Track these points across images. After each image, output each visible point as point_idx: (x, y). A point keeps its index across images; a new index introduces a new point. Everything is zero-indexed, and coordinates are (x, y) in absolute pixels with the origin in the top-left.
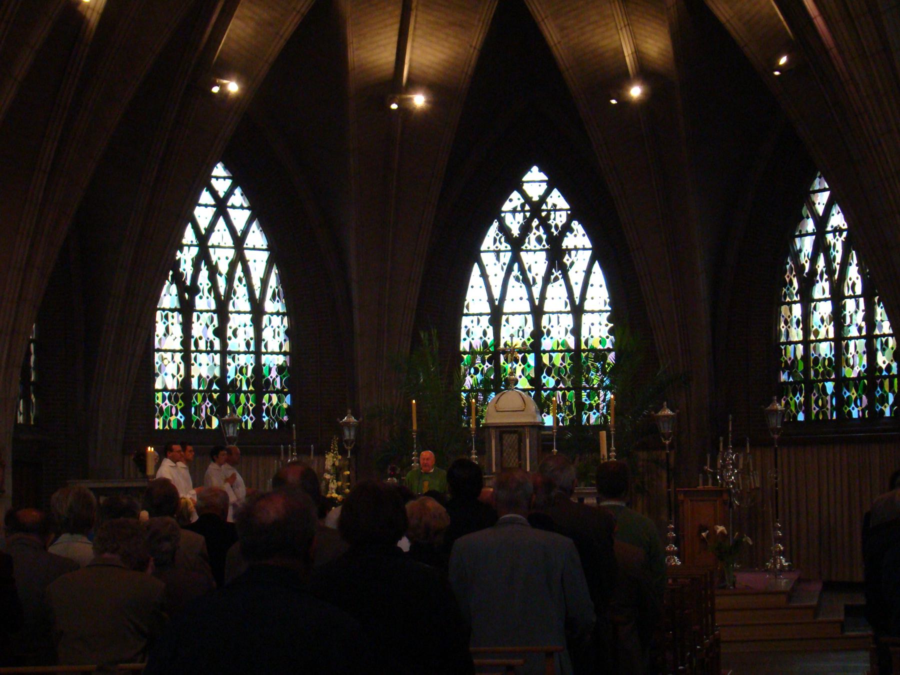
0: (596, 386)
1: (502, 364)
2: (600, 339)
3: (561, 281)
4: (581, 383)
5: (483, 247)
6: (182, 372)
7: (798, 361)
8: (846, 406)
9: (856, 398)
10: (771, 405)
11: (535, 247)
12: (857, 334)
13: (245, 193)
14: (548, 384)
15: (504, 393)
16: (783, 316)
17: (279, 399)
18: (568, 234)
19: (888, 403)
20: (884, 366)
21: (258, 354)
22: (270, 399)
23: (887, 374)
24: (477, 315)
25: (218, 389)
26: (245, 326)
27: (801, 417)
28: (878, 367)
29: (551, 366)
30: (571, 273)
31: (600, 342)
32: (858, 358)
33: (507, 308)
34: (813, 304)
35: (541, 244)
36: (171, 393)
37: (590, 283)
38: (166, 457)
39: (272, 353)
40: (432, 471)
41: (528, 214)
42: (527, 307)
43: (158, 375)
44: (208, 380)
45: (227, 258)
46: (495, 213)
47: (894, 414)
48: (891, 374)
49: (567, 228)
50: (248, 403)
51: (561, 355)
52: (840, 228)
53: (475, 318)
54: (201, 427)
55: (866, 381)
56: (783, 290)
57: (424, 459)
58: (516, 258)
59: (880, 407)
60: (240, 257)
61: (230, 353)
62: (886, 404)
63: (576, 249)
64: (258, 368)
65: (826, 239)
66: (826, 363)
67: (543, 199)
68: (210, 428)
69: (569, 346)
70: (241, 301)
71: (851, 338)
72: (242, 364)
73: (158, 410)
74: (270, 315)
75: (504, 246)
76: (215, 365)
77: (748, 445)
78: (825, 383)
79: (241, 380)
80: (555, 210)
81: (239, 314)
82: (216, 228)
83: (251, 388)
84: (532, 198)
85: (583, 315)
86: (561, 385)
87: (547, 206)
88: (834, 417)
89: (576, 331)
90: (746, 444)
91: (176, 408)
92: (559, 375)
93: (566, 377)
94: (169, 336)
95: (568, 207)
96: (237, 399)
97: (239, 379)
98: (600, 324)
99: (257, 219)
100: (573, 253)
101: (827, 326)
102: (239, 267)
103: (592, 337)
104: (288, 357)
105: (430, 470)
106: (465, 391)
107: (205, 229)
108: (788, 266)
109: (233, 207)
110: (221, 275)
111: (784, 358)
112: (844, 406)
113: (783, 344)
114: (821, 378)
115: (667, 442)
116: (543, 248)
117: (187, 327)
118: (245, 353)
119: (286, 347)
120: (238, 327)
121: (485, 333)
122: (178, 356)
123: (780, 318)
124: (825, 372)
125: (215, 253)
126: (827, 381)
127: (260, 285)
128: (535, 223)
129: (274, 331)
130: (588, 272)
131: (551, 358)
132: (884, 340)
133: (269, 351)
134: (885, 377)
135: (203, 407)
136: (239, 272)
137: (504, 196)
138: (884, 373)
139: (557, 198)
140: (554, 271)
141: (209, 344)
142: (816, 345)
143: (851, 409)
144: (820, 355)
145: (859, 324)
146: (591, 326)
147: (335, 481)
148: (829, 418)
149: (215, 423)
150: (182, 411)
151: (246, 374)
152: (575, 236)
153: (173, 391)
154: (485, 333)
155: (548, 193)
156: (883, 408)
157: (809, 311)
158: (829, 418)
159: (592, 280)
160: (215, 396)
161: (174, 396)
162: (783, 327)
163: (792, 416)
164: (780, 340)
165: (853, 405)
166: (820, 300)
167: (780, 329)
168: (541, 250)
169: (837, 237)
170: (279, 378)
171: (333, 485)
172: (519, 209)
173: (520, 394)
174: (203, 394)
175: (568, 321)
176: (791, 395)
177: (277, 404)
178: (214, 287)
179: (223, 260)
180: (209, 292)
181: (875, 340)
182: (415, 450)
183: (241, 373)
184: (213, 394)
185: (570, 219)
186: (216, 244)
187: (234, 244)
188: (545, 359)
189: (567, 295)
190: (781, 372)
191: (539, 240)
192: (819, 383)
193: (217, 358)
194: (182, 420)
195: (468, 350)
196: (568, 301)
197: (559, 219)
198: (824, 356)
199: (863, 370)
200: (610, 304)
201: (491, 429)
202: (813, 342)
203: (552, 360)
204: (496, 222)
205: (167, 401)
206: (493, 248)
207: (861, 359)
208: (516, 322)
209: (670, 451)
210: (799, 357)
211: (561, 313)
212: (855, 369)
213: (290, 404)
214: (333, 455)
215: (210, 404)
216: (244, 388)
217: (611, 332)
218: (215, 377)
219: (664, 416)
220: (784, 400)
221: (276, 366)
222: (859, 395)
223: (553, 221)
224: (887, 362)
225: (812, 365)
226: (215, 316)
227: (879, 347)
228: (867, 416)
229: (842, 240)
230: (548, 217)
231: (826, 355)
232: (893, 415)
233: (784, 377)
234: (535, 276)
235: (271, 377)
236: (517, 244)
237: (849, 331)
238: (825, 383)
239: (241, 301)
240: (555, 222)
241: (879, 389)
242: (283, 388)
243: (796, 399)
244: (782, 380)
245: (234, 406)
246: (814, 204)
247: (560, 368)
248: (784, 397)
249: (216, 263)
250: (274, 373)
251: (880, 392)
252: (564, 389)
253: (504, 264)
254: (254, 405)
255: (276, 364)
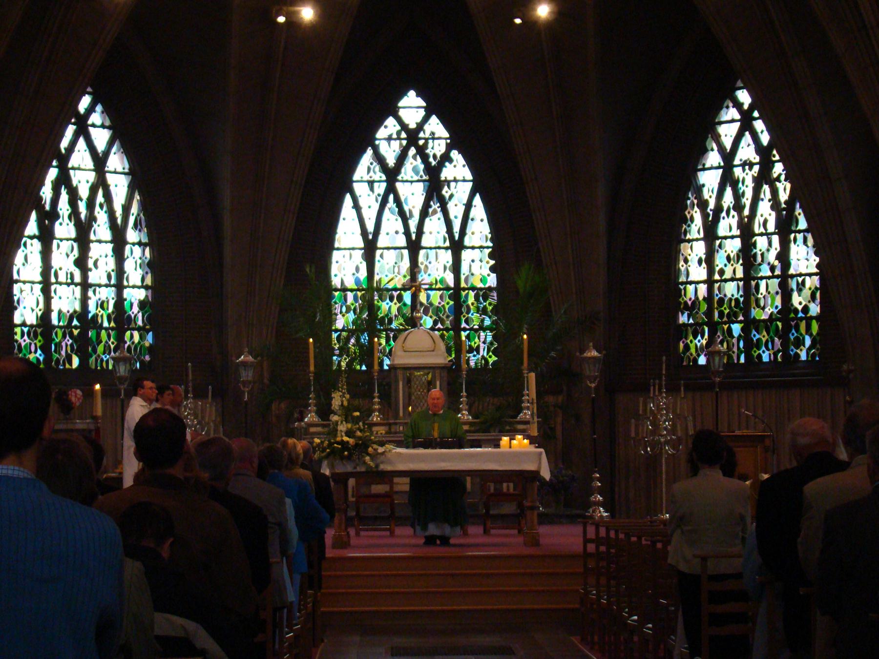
0: (476, 327)
1: (376, 302)
2: (481, 276)
3: (440, 215)
4: (460, 324)
5: (356, 177)
6: (41, 306)
7: (699, 302)
8: (755, 349)
9: (767, 341)
10: (712, 346)
11: (412, 177)
12: (769, 274)
13: (106, 111)
14: (426, 324)
15: (411, 332)
16: (683, 255)
17: (141, 337)
18: (447, 164)
19: (804, 346)
20: (800, 308)
21: (120, 287)
22: (132, 336)
23: (803, 316)
24: (349, 249)
25: (78, 324)
26: (106, 256)
27: (702, 360)
28: (792, 308)
29: (429, 305)
30: (450, 206)
31: (481, 280)
32: (769, 299)
33: (381, 243)
34: (718, 242)
35: (418, 175)
36: (30, 329)
37: (471, 216)
38: (136, 395)
39: (134, 287)
40: (441, 412)
41: (404, 142)
42: (402, 241)
43: (16, 308)
44: (68, 314)
45: (88, 182)
46: (369, 141)
47: (811, 357)
48: (808, 315)
49: (446, 158)
50: (109, 340)
51: (439, 293)
52: (750, 162)
53: (347, 252)
54: (61, 366)
55: (780, 324)
56: (682, 227)
57: (434, 399)
58: (391, 189)
59: (795, 350)
60: (101, 183)
61: (91, 286)
62: (802, 347)
63: (455, 180)
64: (120, 301)
65: (734, 173)
66: (733, 304)
67: (420, 127)
68: (70, 367)
69: (448, 285)
70: (102, 230)
71: (762, 278)
72: (104, 298)
73: (16, 347)
74: (132, 246)
75: (379, 175)
76: (76, 299)
77: (682, 388)
78: (731, 325)
79: (102, 316)
80: (433, 139)
81: (100, 243)
82: (76, 149)
83: (113, 324)
84: (408, 125)
85: (463, 251)
86: (439, 326)
87: (424, 133)
88: (742, 360)
89: (456, 268)
90: (680, 388)
91: (35, 344)
92: (437, 315)
93: (444, 317)
94: (28, 265)
95: (447, 135)
96: (98, 335)
97: (100, 314)
98: (481, 261)
99: (118, 140)
100: (453, 184)
101: (735, 265)
102: (100, 192)
103: (472, 274)
104: (150, 291)
105: (439, 411)
106: (336, 331)
107: (65, 149)
108: (689, 202)
109: (93, 125)
110: (82, 200)
111: (683, 299)
112: (753, 348)
113: (682, 283)
114: (727, 320)
115: (593, 385)
116: (420, 179)
117: (46, 254)
118: (107, 286)
119: (149, 281)
120: (99, 258)
121: (357, 269)
122: (38, 288)
123: (679, 256)
124: (732, 313)
125: (75, 176)
126: (734, 322)
127: (121, 212)
128: (412, 151)
129: (136, 262)
130: (469, 206)
131: (428, 297)
132: (800, 279)
133: (131, 284)
134: (801, 319)
135: (64, 344)
136: (100, 198)
137: (379, 123)
138: (800, 315)
139: (435, 125)
140: (432, 203)
141: (69, 276)
142: (722, 285)
143: (761, 352)
144: (725, 295)
145: (772, 263)
146: (471, 263)
147: (344, 423)
148: (736, 362)
149: (76, 362)
150: (41, 348)
151: (108, 309)
152: (455, 166)
153: (31, 326)
154: (357, 269)
155: (426, 119)
156: (798, 351)
157: (713, 249)
158: (736, 362)
159: (472, 214)
160: (76, 332)
161: (33, 330)
162: (682, 266)
163: (692, 359)
164: (679, 279)
165: (764, 348)
166: (726, 238)
167: (679, 269)
168: (418, 181)
169: (747, 170)
170: (140, 314)
171: (343, 427)
172: (395, 136)
173: (428, 333)
174: (63, 330)
175: (447, 257)
176: (691, 338)
177: (139, 343)
178: (75, 213)
179: (84, 182)
180: (70, 218)
181: (789, 279)
182: (313, 393)
183: (102, 307)
184: (74, 330)
185: (449, 148)
186: (76, 166)
187: (94, 166)
188: (423, 297)
189: (446, 230)
190: (680, 313)
191: (415, 170)
192: (724, 325)
193: (78, 290)
194: (41, 358)
195: (339, 287)
196: (447, 236)
197: (437, 148)
198: (731, 297)
199: (775, 311)
200: (492, 240)
201: (398, 371)
202: (717, 281)
203: (429, 299)
204: (370, 150)
205: (26, 337)
206: (367, 178)
207: (773, 300)
208: (390, 257)
209: (720, 390)
210: (701, 298)
211: (439, 248)
212: (767, 310)
213: (151, 343)
214: (341, 394)
215: (71, 341)
216: (106, 324)
217: (493, 269)
218: (75, 312)
219: (590, 358)
220: (683, 342)
221: (138, 301)
222: (771, 337)
223: (432, 150)
224: (804, 303)
225: (716, 306)
226: (75, 245)
227: (794, 286)
228: (780, 360)
229: (753, 176)
230: (426, 145)
231: (733, 295)
232: (810, 359)
233: (683, 319)
234: (411, 208)
235: (133, 313)
236: (392, 174)
237: (760, 270)
238: (731, 325)
239: (102, 230)
240: (433, 152)
241: (793, 331)
242: (145, 325)
243: (696, 341)
244: (681, 322)
245: (95, 343)
246: (720, 136)
247: (438, 307)
248: (684, 339)
249: (77, 185)
250: (136, 309)
251: (796, 335)
252: (443, 330)
253: (379, 195)
254: (116, 343)
255: (138, 298)
